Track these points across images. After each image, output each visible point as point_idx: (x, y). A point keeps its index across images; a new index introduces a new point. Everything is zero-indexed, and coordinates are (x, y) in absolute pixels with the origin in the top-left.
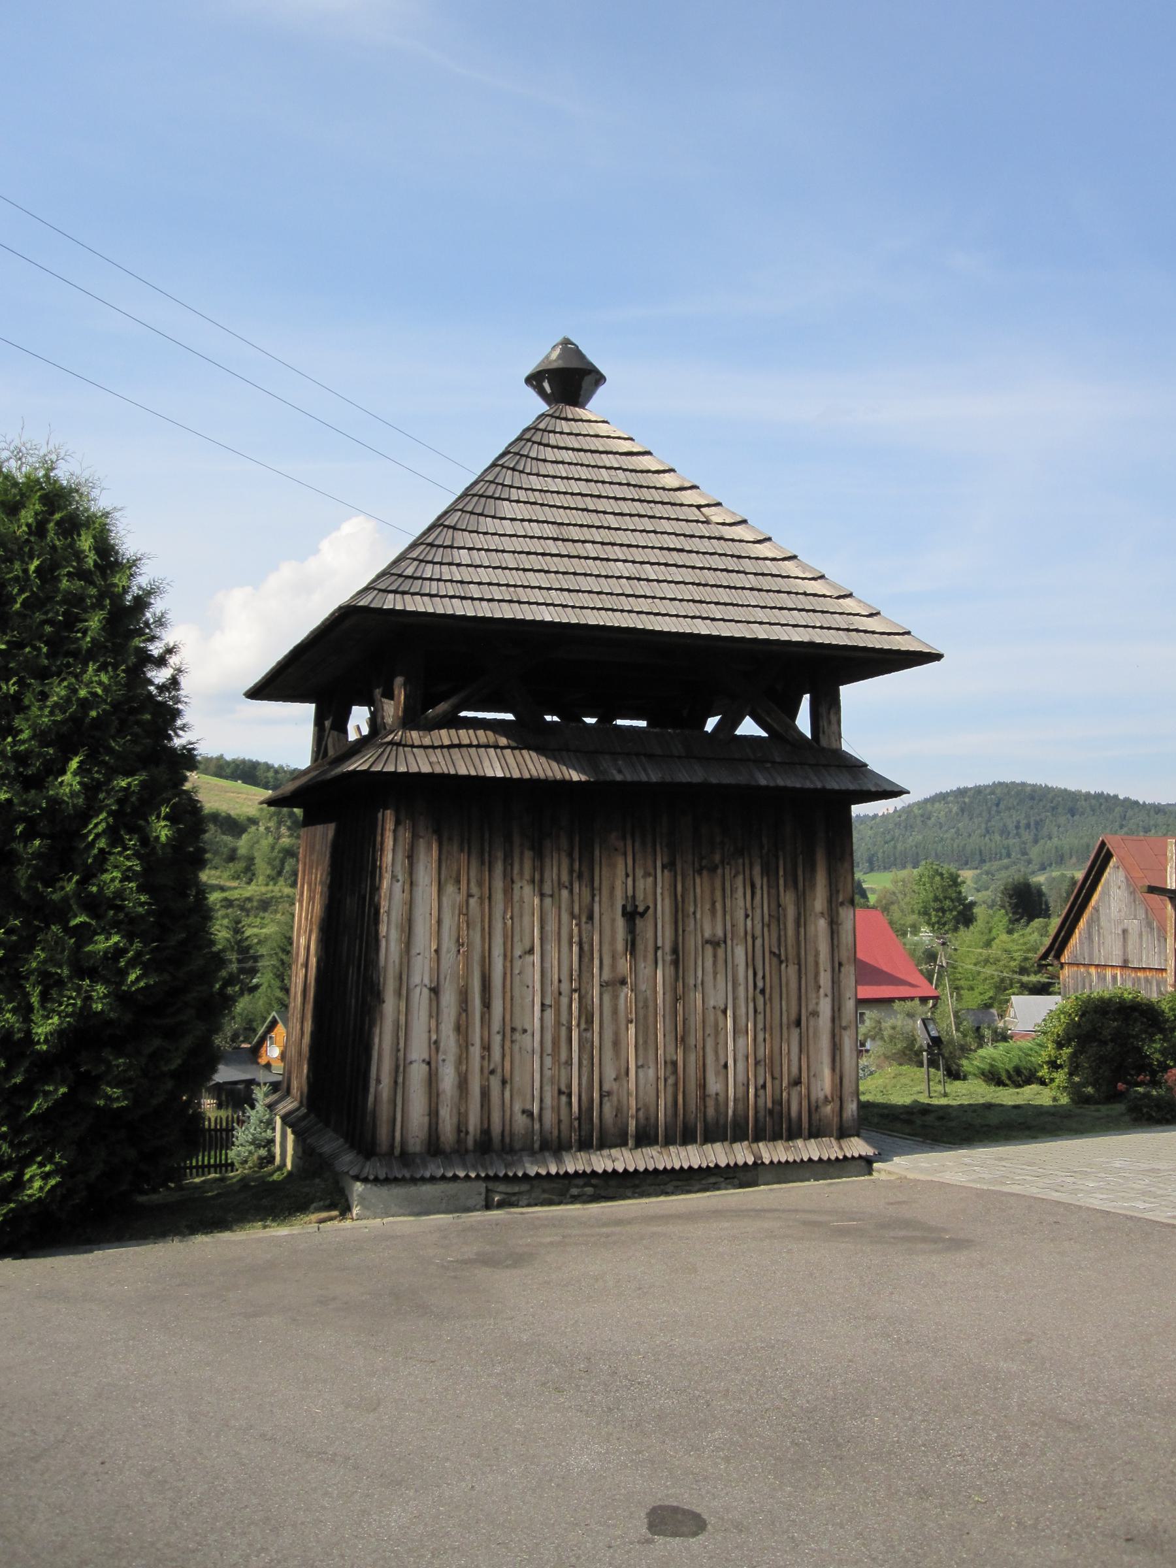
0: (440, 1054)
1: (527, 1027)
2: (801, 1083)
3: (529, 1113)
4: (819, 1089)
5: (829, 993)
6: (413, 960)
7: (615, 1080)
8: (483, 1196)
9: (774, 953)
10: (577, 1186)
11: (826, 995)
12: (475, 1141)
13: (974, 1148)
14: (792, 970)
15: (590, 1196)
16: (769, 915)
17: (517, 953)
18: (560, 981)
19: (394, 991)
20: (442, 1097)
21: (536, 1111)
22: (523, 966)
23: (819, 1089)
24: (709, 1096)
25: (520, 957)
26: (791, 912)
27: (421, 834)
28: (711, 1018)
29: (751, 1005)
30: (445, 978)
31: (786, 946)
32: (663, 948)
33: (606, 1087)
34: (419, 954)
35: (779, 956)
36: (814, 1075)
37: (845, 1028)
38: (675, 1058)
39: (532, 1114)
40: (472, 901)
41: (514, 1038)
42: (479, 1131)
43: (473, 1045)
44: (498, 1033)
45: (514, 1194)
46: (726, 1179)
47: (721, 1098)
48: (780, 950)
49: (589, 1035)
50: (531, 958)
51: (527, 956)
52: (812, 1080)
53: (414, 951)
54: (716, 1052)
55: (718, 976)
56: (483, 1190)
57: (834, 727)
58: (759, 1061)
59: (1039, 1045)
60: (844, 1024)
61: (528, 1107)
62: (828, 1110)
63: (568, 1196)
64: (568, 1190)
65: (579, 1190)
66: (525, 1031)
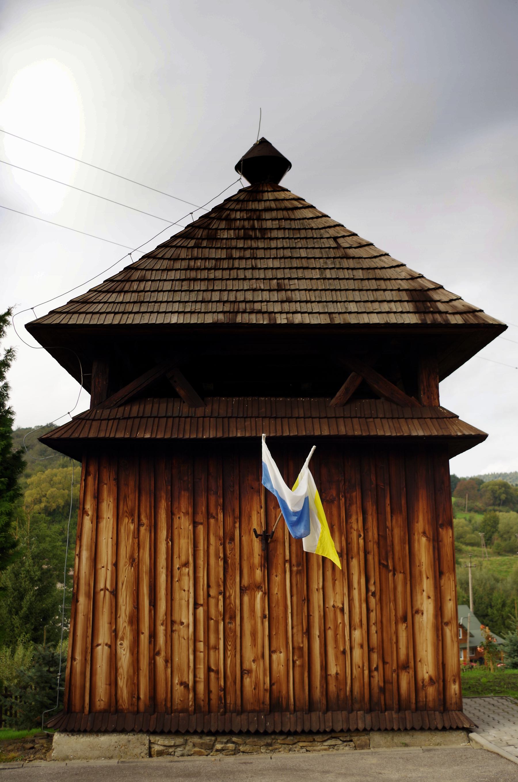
0: (118, 640)
1: (184, 620)
2: (408, 667)
3: (185, 685)
4: (425, 671)
5: (432, 594)
6: (99, 571)
7: (254, 661)
8: (147, 746)
9: (383, 564)
10: (222, 743)
11: (429, 597)
12: (145, 705)
13: (495, 476)
14: (391, 574)
15: (232, 751)
16: (379, 535)
17: (177, 565)
18: (209, 586)
19: (85, 594)
20: (120, 671)
21: (191, 684)
22: (181, 575)
23: (425, 671)
24: (330, 675)
25: (179, 569)
26: (397, 533)
27: (106, 482)
28: (330, 615)
29: (364, 606)
30: (123, 584)
31: (393, 559)
32: (290, 561)
33: (246, 666)
34: (103, 567)
35: (387, 567)
36: (420, 661)
37: (447, 624)
38: (302, 646)
39: (188, 685)
40: (142, 529)
41: (174, 628)
42: (148, 698)
43: (143, 633)
44: (162, 624)
45: (171, 746)
46: (344, 742)
47: (341, 677)
48: (387, 562)
49: (232, 626)
50: (187, 570)
51: (184, 568)
52: (419, 664)
53: (99, 566)
54: (336, 641)
55: (337, 582)
56: (147, 742)
57: (437, 401)
58: (373, 649)
59: (481, 660)
60: (446, 620)
61: (185, 679)
62: (431, 691)
63: (214, 750)
64: (214, 745)
65: (222, 746)
66: (182, 623)
